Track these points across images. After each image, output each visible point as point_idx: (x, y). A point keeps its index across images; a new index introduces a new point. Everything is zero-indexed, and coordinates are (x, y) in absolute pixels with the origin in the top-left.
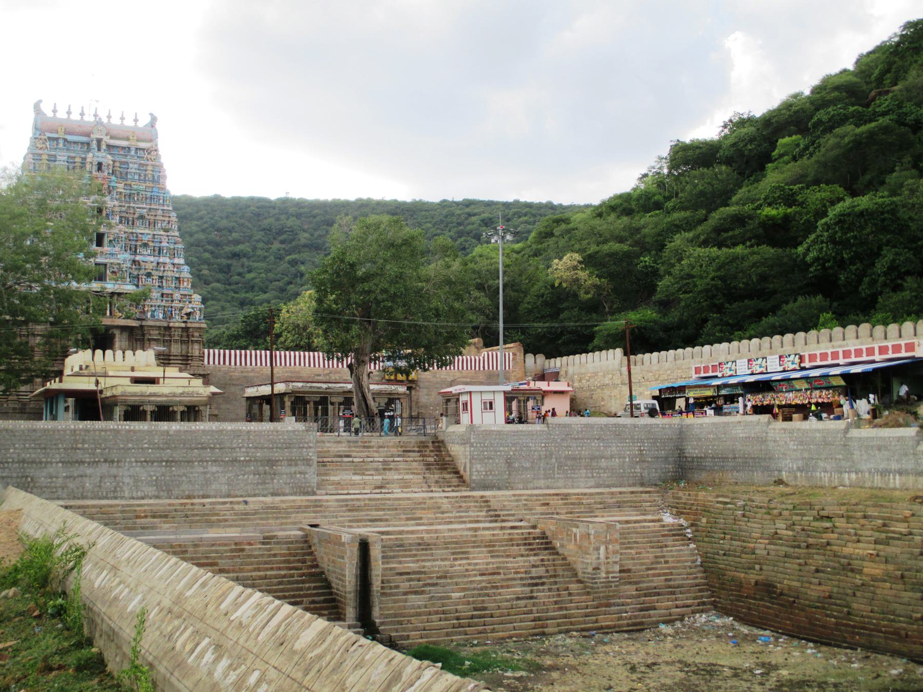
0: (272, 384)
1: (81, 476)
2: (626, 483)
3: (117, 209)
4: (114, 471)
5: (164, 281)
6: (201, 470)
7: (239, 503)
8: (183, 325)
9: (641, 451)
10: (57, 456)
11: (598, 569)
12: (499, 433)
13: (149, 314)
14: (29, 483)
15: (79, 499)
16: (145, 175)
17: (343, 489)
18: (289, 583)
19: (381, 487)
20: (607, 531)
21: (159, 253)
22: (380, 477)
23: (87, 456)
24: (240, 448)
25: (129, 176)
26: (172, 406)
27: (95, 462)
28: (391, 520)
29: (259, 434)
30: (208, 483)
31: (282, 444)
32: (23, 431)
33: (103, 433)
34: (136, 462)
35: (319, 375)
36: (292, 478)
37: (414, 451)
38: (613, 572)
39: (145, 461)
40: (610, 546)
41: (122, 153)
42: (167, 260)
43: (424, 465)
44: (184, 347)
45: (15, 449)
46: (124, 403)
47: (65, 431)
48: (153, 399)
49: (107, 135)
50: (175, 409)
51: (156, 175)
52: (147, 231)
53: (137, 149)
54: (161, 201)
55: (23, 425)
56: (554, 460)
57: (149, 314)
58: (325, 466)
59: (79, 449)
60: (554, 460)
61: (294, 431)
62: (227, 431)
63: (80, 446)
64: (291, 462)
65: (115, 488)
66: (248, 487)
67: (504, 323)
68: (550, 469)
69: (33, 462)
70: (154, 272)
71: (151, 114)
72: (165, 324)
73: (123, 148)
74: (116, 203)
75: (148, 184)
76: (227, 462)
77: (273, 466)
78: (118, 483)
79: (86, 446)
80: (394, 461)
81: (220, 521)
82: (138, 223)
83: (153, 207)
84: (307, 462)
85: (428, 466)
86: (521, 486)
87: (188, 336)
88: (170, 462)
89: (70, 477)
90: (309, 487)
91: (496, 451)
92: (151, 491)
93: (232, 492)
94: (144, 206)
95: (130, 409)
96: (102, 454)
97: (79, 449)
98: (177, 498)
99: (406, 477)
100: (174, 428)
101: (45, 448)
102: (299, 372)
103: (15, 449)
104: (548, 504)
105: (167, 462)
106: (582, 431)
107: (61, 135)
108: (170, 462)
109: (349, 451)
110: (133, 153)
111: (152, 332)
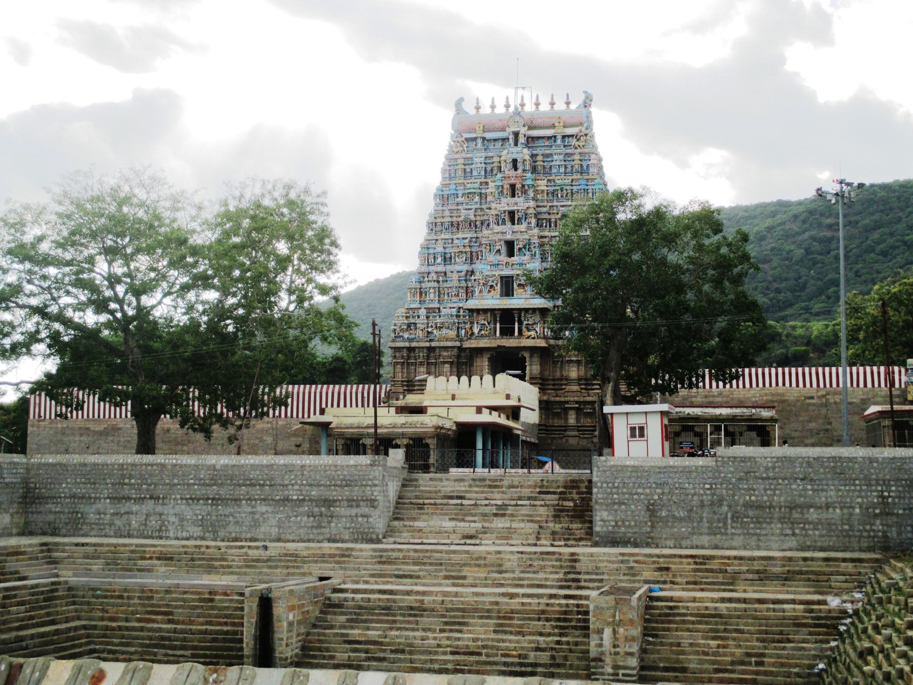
0: (892, 405)
1: (128, 513)
2: (856, 545)
4: (159, 509)
6: (250, 509)
7: (257, 548)
9: (883, 497)
10: (106, 491)
11: (601, 660)
14: (79, 519)
15: (125, 537)
17: (427, 538)
18: (225, 640)
19: (471, 537)
20: (615, 608)
24: (293, 485)
25: (554, 170)
26: (393, 440)
27: (140, 498)
28: (424, 577)
29: (315, 469)
30: (256, 524)
31: (342, 480)
32: (75, 465)
33: (149, 468)
34: (182, 499)
35: (812, 398)
37: (554, 493)
38: (625, 668)
39: (191, 498)
40: (621, 630)
41: (547, 144)
43: (555, 510)
45: (68, 483)
47: (113, 465)
51: (585, 164)
53: (564, 137)
54: (590, 195)
56: (725, 509)
58: (421, 509)
59: (126, 484)
60: (725, 509)
62: (278, 466)
63: (127, 481)
64: (352, 502)
65: (161, 527)
66: (302, 531)
68: (719, 521)
69: (83, 497)
71: (585, 92)
73: (549, 138)
74: (532, 204)
75: (574, 177)
77: (329, 507)
78: (163, 522)
79: (133, 481)
81: (222, 566)
86: (671, 543)
89: (117, 514)
90: (372, 533)
92: (197, 531)
93: (283, 536)
94: (569, 203)
95: (411, 442)
96: (148, 490)
97: (126, 484)
98: (223, 541)
99: (514, 525)
100: (222, 462)
101: (94, 483)
102: (783, 395)
103: (68, 483)
104: (667, 569)
105: (213, 499)
106: (774, 468)
107: (479, 134)
109: (466, 492)
110: (559, 141)
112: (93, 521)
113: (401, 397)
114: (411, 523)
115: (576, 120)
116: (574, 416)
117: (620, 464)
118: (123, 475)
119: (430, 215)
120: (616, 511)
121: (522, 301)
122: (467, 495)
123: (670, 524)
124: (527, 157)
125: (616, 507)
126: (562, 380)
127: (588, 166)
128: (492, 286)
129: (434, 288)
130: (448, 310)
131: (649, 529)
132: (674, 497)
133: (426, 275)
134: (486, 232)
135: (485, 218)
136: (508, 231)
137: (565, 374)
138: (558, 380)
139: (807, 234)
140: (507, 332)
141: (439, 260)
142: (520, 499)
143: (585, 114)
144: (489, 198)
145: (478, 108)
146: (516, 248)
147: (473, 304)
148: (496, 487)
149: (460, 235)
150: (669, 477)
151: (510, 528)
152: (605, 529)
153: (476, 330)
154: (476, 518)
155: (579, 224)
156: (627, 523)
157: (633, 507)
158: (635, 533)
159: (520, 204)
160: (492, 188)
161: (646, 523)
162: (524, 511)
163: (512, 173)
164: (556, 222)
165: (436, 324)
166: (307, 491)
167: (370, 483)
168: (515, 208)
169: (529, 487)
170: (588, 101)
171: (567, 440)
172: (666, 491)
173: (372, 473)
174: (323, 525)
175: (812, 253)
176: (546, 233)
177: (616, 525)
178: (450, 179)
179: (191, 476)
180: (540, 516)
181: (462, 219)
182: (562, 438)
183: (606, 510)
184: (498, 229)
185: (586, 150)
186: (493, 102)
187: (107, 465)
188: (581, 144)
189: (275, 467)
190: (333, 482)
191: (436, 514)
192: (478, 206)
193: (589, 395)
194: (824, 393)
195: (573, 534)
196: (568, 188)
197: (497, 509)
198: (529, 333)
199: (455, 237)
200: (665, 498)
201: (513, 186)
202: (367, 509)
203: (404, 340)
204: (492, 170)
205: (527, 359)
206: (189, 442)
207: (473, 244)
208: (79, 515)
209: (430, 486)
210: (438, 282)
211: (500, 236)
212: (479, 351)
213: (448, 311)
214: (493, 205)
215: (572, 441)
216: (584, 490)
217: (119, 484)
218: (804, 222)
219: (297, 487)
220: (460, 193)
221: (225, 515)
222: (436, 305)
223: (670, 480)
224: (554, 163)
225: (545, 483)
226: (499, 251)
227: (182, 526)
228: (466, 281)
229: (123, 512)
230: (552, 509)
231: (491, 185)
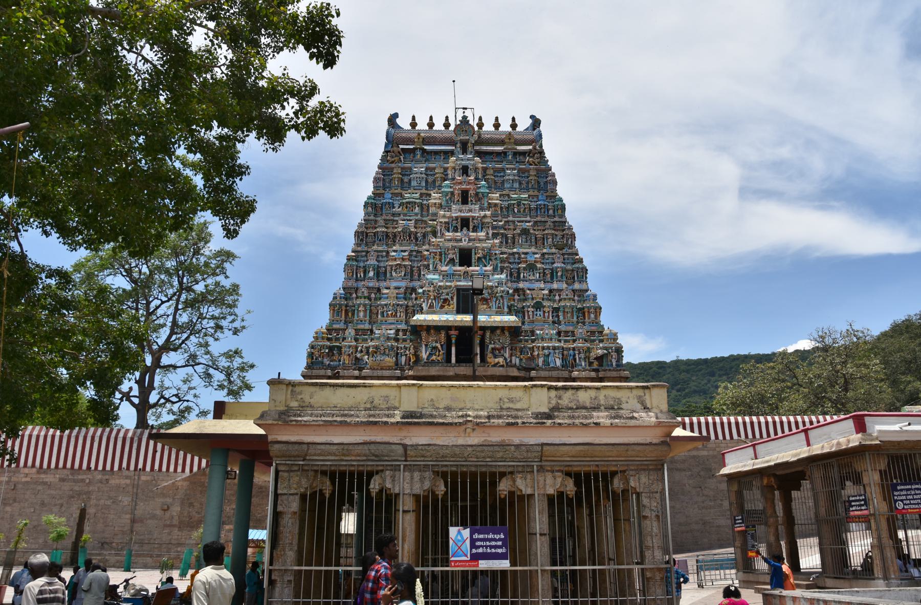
5: (560, 314)
13: (541, 361)
16: (528, 183)
21: (552, 278)
25: (507, 185)
48: (420, 437)
50: (523, 485)
54: (551, 212)
67: (585, 565)
70: (545, 303)
71: (532, 117)
94: (528, 219)
128: (445, 300)
129: (365, 305)
133: (353, 291)
136: (464, 238)
141: (371, 274)
153: (424, 355)
159: (474, 211)
164: (514, 238)
184: (449, 235)
192: (419, 217)
198: (497, 360)
204: (434, 181)
206: (15, 501)
207: (413, 258)
210: (370, 299)
222: (367, 326)
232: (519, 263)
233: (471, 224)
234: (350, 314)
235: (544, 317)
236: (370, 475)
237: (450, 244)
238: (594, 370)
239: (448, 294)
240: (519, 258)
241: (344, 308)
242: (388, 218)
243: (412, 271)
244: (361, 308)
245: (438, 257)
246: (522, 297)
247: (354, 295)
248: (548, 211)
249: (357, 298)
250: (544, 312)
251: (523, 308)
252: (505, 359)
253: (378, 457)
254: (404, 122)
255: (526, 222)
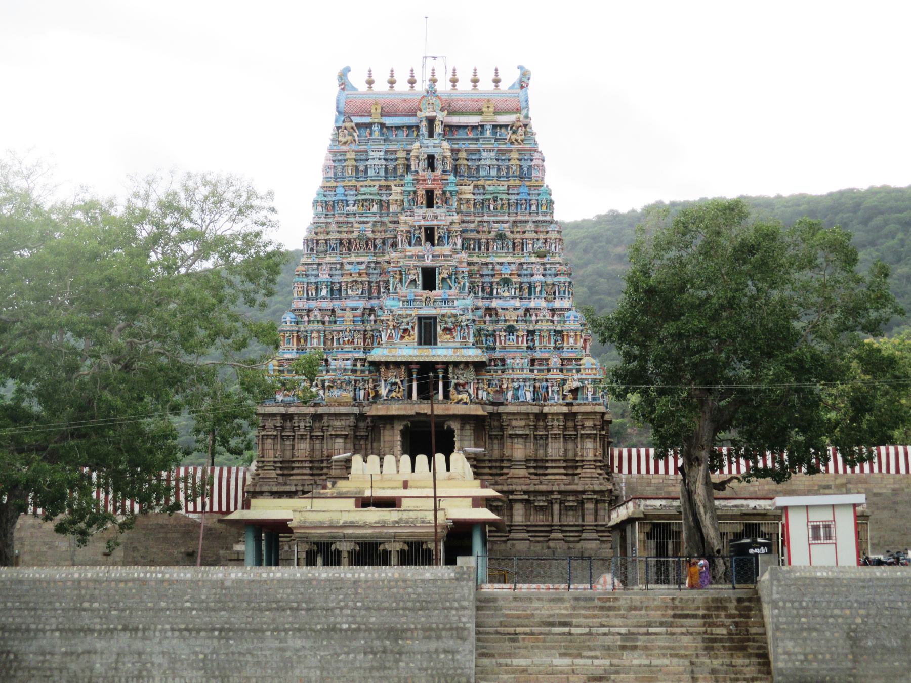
1: (89, 652)
3: (456, 227)
4: (138, 645)
5: (537, 338)
6: (277, 644)
8: (565, 409)
12: (850, 585)
13: (510, 394)
14: (11, 661)
16: (508, 168)
21: (530, 294)
22: (607, 662)
23: (98, 620)
24: (341, 608)
25: (482, 173)
27: (108, 630)
29: (373, 585)
31: (414, 601)
33: (122, 585)
34: (173, 630)
36: (431, 659)
37: (695, 616)
39: (186, 630)
41: (471, 135)
42: (543, 304)
43: (704, 640)
44: (570, 445)
46: (304, 539)
49: (442, 110)
50: (388, 547)
52: (509, 259)
53: (494, 127)
55: (185, 573)
57: (510, 394)
58: (513, 640)
59: (84, 610)
61: (435, 580)
62: (319, 581)
63: (86, 605)
64: (430, 633)
65: (140, 672)
66: (355, 674)
69: (17, 630)
70: (518, 326)
71: (521, 68)
72: (536, 410)
73: (474, 128)
74: (456, 218)
75: (512, 182)
76: (320, 631)
77: (396, 640)
79: (96, 605)
80: (648, 634)
82: (495, 246)
83: (519, 218)
84: (459, 632)
85: (710, 644)
87: (575, 428)
88: (225, 632)
89: (72, 653)
91: (825, 617)
94: (506, 218)
95: (406, 548)
96: (119, 618)
97: (84, 610)
99: (656, 662)
100: (233, 576)
101: (35, 609)
105: (221, 630)
108: (225, 632)
109: (571, 615)
110: (488, 133)
111: (514, 423)
112: (33, 664)
113: (329, 484)
114: (509, 661)
115: (512, 105)
116: (521, 512)
117: (808, 575)
118: (80, 596)
119: (309, 230)
120: (805, 640)
121: (451, 352)
122: (574, 621)
123: (878, 657)
124: (449, 153)
125: (805, 634)
126: (502, 461)
127: (530, 168)
128: (406, 330)
129: (318, 331)
130: (341, 361)
131: (850, 665)
132: (883, 621)
133: (304, 313)
134: (394, 255)
135: (389, 235)
136: (427, 255)
137: (507, 453)
138: (496, 461)
139: (590, 268)
140: (426, 393)
141: (324, 293)
142: (649, 625)
143: (522, 98)
144: (393, 208)
145: (370, 83)
146: (438, 278)
147: (378, 354)
148: (610, 608)
149: (353, 259)
150: (876, 593)
151: (650, 666)
152: (790, 665)
153: (383, 391)
154: (598, 653)
155: (206, 248)
156: (820, 657)
157: (828, 634)
158: (831, 670)
159: (440, 217)
160: (396, 193)
161: (846, 655)
162: (661, 642)
163: (428, 174)
165: (323, 382)
166: (363, 617)
167: (456, 605)
168: (435, 223)
169: (657, 608)
170: (525, 80)
171: (513, 545)
172: (873, 612)
173: (459, 590)
174: (387, 665)
175: (597, 293)
176: (475, 259)
177: (806, 660)
178: (336, 179)
179: (186, 598)
180: (686, 648)
181: (355, 235)
182: (505, 542)
183: (791, 639)
185: (528, 147)
186: (433, 74)
187: (55, 582)
188: (519, 138)
189: (314, 583)
190: (401, 604)
191: (538, 647)
192: (377, 218)
193: (541, 483)
194: (844, 481)
195: (741, 672)
196: (503, 197)
197: (622, 640)
198: (460, 397)
199: (345, 261)
200: (871, 621)
201: (430, 194)
202: (451, 642)
203: (277, 404)
204: (395, 169)
205: (456, 432)
207: (371, 271)
208: (12, 656)
209: (516, 608)
210: (323, 323)
211: (414, 261)
212: (390, 420)
213: (340, 364)
214: (402, 218)
215: (522, 546)
216: (734, 612)
217: (75, 609)
218: (585, 251)
219: (349, 612)
220: (351, 200)
221: (240, 653)
223: (877, 597)
224: (482, 163)
225: (677, 603)
226: (414, 281)
227: (173, 669)
228: (363, 322)
229: (80, 650)
230: (699, 638)
231: (396, 189)
232: (493, 276)
233: (436, 233)
234: (302, 341)
235: (518, 342)
236: (331, 544)
237: (414, 261)
238: (568, 404)
239: (408, 324)
240: (493, 269)
241: (295, 334)
242: (341, 220)
243: (370, 287)
244: (315, 335)
245: (398, 276)
246: (494, 318)
247: (306, 318)
248: (530, 206)
249: (309, 322)
250: (518, 336)
251: (495, 331)
252: (470, 395)
253: (334, 537)
254: (358, 81)
255: (503, 222)
